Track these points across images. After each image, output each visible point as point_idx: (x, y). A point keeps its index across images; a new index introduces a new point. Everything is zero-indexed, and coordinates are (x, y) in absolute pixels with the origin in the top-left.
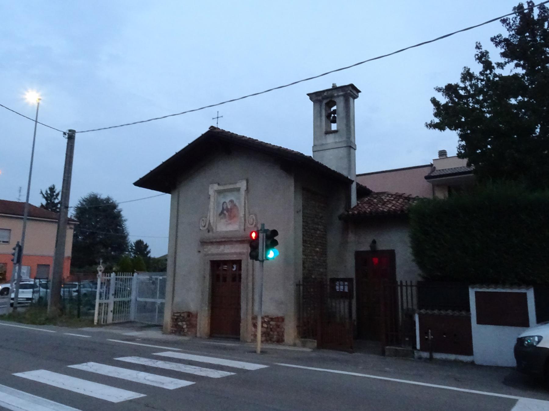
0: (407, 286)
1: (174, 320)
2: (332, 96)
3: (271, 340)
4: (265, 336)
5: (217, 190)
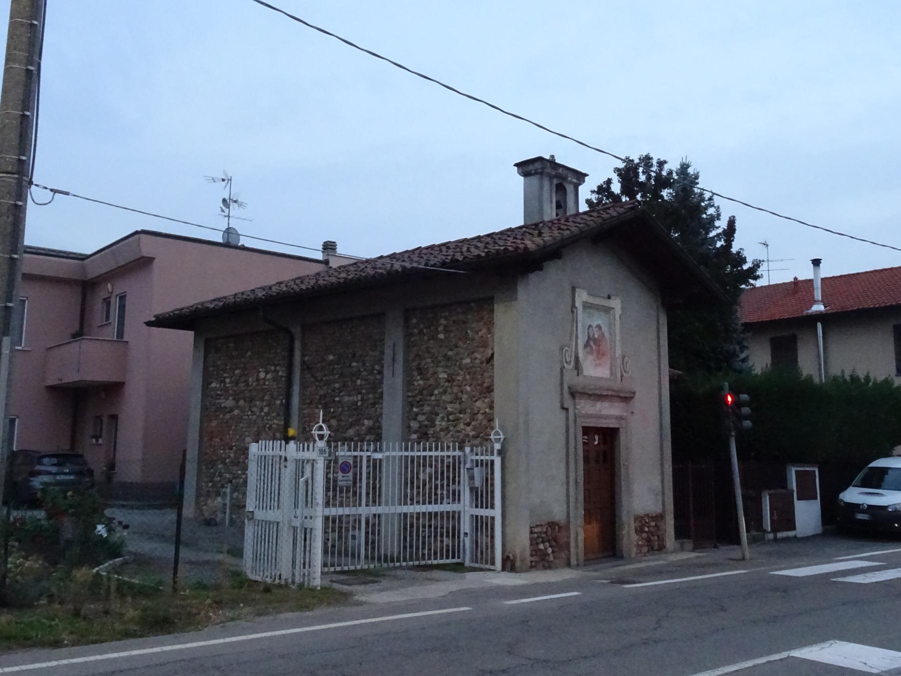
2: (565, 179)
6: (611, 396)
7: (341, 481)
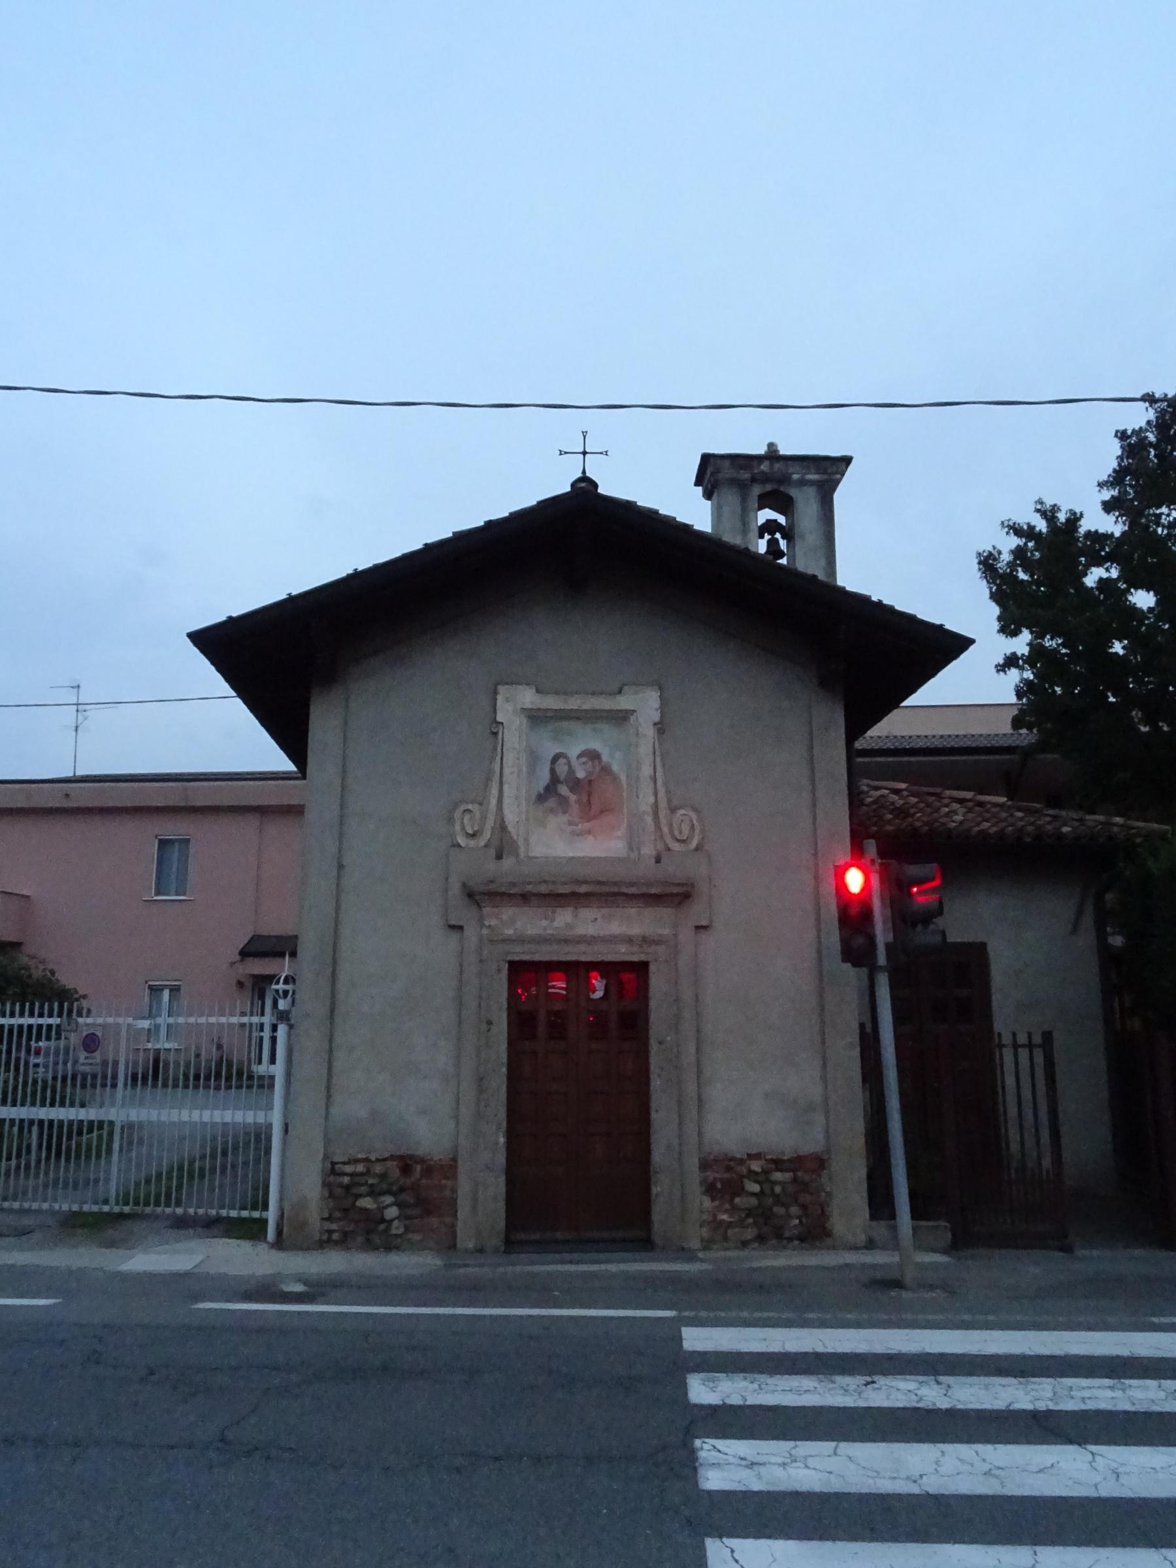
0: (1030, 1046)
1: (339, 1191)
2: (785, 479)
3: (779, 1236)
4: (755, 1224)
5: (531, 709)
6: (588, 895)
7: (83, 1064)
